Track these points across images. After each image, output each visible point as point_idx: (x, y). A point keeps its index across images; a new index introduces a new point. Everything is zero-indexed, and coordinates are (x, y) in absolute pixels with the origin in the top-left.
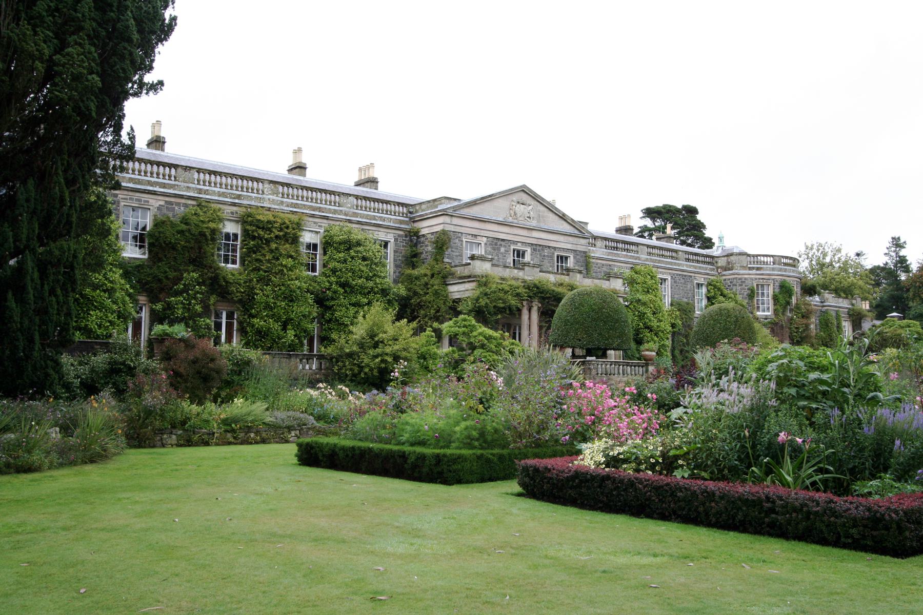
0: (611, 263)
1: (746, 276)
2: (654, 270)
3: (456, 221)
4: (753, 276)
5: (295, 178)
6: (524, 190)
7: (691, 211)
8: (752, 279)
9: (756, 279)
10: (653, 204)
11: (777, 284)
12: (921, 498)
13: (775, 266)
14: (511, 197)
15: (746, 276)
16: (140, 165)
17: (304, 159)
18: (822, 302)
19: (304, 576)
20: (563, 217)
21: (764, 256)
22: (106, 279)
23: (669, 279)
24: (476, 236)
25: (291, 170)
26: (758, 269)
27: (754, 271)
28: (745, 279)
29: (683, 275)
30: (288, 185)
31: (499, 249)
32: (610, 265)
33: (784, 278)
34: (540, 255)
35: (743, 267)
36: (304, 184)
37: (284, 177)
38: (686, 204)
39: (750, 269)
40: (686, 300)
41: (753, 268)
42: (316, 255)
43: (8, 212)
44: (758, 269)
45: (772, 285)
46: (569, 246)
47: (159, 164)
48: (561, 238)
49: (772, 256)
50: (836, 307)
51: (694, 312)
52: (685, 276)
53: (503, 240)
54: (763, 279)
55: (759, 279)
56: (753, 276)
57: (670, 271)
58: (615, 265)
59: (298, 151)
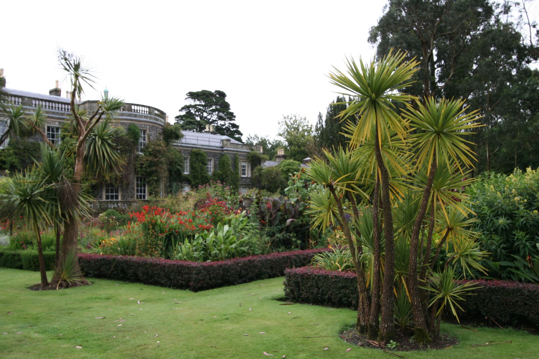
5: (54, 97)
7: (222, 95)
10: (195, 90)
13: (124, 112)
16: (18, 99)
18: (222, 147)
19: (414, 325)
21: (137, 105)
25: (51, 92)
30: (52, 102)
33: (133, 122)
36: (60, 101)
37: (48, 97)
42: (245, 170)
43: (475, 199)
47: (58, 103)
49: (149, 107)
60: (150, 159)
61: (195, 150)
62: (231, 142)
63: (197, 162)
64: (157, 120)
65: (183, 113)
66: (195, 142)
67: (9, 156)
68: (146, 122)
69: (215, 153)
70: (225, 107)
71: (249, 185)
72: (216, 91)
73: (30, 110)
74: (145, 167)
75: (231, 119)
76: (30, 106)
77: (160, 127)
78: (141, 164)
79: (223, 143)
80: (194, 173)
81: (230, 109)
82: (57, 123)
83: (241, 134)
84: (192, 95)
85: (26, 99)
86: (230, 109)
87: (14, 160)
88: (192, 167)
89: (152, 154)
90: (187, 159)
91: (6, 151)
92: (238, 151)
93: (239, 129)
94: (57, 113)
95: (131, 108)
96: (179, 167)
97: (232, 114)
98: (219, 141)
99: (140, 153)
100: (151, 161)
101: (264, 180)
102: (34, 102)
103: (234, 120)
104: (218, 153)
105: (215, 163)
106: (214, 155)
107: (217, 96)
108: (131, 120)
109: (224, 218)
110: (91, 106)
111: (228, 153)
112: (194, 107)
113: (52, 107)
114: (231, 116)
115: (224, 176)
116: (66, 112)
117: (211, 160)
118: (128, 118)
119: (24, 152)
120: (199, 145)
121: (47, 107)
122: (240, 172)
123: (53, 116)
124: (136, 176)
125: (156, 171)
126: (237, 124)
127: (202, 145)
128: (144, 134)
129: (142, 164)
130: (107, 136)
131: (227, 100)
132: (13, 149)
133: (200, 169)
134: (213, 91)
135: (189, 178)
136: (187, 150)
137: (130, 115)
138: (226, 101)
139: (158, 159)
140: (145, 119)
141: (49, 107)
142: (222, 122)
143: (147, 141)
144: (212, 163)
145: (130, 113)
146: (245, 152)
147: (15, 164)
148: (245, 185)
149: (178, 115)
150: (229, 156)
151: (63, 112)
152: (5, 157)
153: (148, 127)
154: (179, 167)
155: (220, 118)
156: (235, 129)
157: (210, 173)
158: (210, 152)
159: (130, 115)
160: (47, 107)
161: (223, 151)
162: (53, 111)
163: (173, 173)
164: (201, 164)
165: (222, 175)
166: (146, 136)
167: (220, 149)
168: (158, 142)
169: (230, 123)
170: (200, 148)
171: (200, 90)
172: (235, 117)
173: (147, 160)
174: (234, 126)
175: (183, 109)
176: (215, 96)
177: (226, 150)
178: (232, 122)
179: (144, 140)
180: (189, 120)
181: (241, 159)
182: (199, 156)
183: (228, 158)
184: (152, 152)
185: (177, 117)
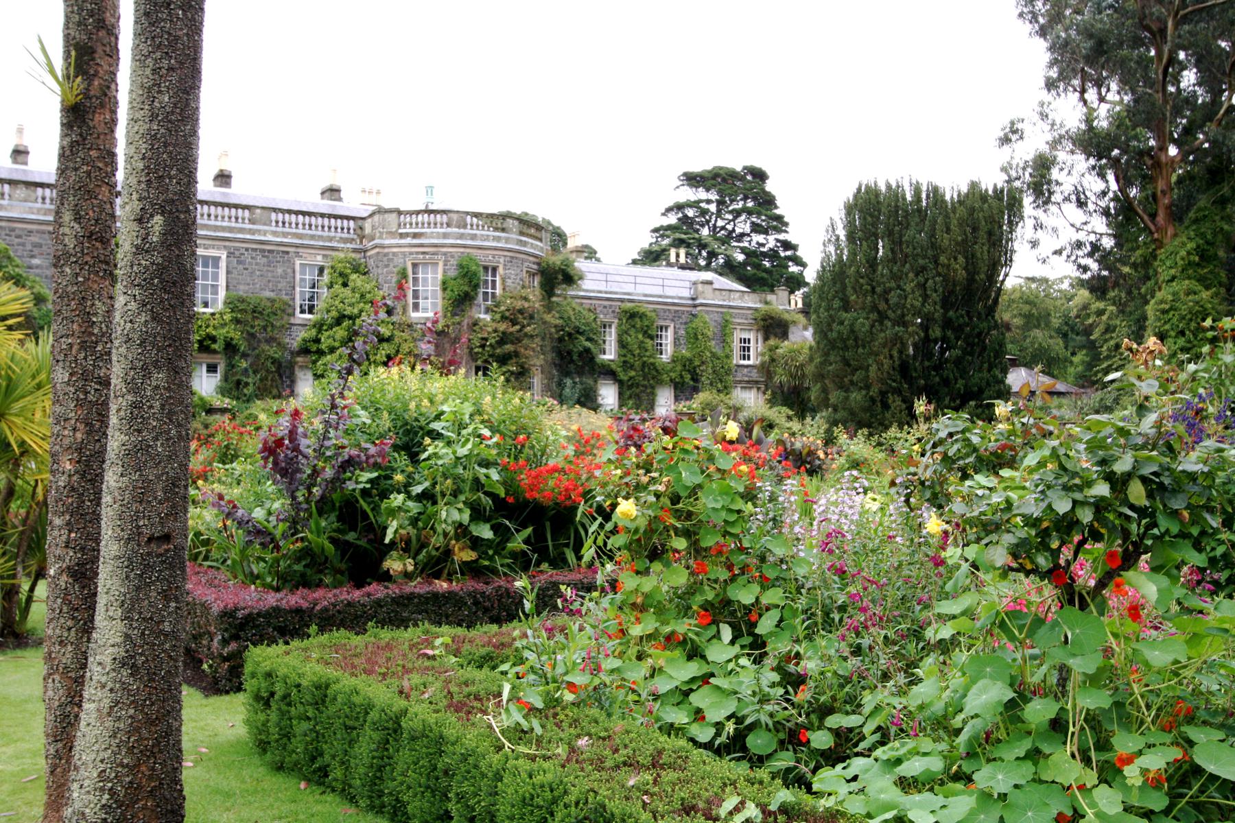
1: (395, 250)
4: (406, 250)
5: (326, 206)
8: (404, 254)
9: (411, 253)
10: (697, 167)
11: (453, 262)
12: (492, 820)
13: (449, 230)
15: (395, 250)
17: (27, 141)
18: (693, 299)
23: (224, 257)
26: (415, 236)
27: (409, 240)
28: (394, 254)
29: (264, 251)
35: (392, 234)
38: (748, 164)
39: (402, 236)
40: (268, 294)
41: (407, 235)
44: (415, 236)
45: (441, 264)
50: (721, 306)
51: (293, 315)
52: (269, 251)
54: (424, 253)
55: (417, 253)
57: (227, 244)
59: (20, 131)
60: (502, 327)
61: (629, 305)
62: (716, 286)
63: (632, 332)
64: (525, 244)
65: (672, 219)
66: (629, 288)
67: (223, 325)
68: (496, 249)
69: (676, 311)
70: (768, 201)
71: (757, 382)
72: (745, 168)
73: (265, 233)
74: (491, 345)
75: (779, 231)
76: (265, 224)
77: (531, 259)
78: (483, 339)
79: (696, 289)
80: (625, 356)
81: (776, 207)
82: (319, 258)
83: (804, 265)
84: (693, 179)
85: (258, 211)
86: (776, 207)
87: (232, 335)
88: (622, 344)
89: (507, 318)
90: (610, 326)
91: (217, 316)
92: (730, 307)
93: (798, 253)
94: (321, 238)
95: (465, 221)
96: (588, 344)
97: (779, 218)
98: (688, 284)
99: (482, 316)
100: (504, 333)
101: (779, 370)
102: (273, 216)
103: (786, 232)
104: (683, 312)
105: (675, 333)
106: (676, 316)
107: (749, 178)
108: (465, 246)
109: (212, 369)
110: (384, 220)
111: (707, 312)
112: (695, 204)
113: (310, 225)
114: (779, 223)
115: (697, 363)
116: (339, 235)
117: (667, 328)
118: (459, 242)
119: (254, 318)
120: (638, 295)
121: (300, 226)
122: (736, 352)
123: (312, 243)
124: (474, 365)
125: (516, 354)
126: (794, 242)
127: (646, 295)
128: (494, 275)
129: (486, 339)
130: (850, 266)
131: (770, 186)
132: (232, 311)
133: (640, 347)
134: (739, 168)
135: (613, 366)
136: (611, 306)
137: (461, 236)
138: (767, 189)
139: (518, 327)
140: (494, 244)
141: (304, 225)
142: (760, 238)
143: (498, 291)
144: (670, 334)
145: (462, 231)
146: (749, 308)
147: (234, 342)
148: (748, 382)
149: (658, 225)
150: (707, 318)
151: (332, 234)
152: (215, 328)
153: (502, 260)
154: (588, 344)
155: (756, 229)
156: (789, 253)
157: (665, 358)
158: (665, 311)
159: (461, 236)
160: (300, 226)
161: (695, 306)
162: (313, 232)
163: (575, 357)
164: (640, 336)
165: (691, 361)
166: (498, 279)
167: (690, 302)
168: (524, 293)
169: (778, 240)
170: (640, 301)
171: (709, 168)
172: (786, 224)
173: (495, 331)
174: (787, 245)
175: (669, 210)
176: (742, 179)
177: (702, 305)
178: (782, 237)
179: (494, 287)
180: (678, 235)
181: (739, 324)
182: (637, 320)
183: (705, 323)
184: (507, 314)
185: (656, 230)
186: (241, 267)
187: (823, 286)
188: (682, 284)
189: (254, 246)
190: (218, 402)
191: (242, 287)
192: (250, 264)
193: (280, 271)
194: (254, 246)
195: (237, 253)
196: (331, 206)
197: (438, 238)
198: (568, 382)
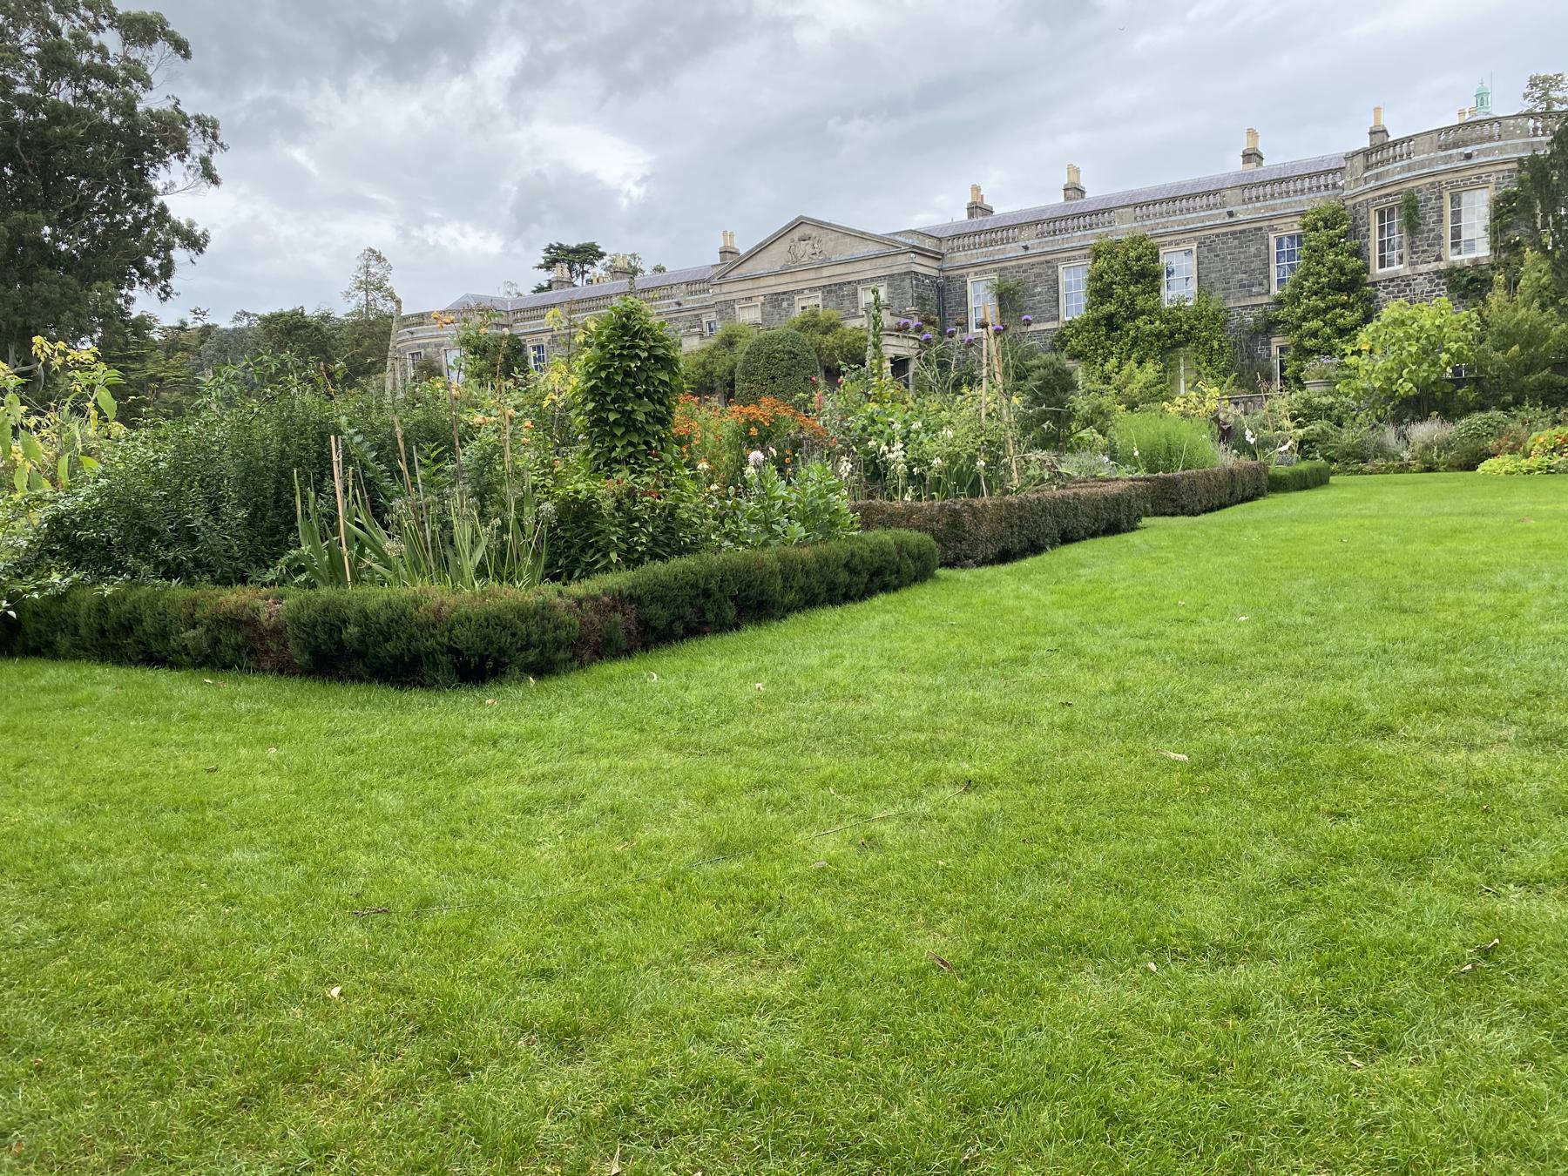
0: (1049, 258)
2: (401, 395)
3: (726, 288)
4: (1370, 195)
5: (980, 221)
6: (800, 223)
9: (1374, 199)
14: (789, 237)
20: (863, 237)
22: (876, 346)
24: (750, 298)
29: (1235, 233)
31: (780, 305)
32: (1047, 262)
34: (837, 297)
44: (1377, 177)
46: (880, 273)
48: (867, 265)
53: (784, 293)
54: (1387, 195)
55: (1380, 197)
56: (1370, 195)
57: (1197, 234)
58: (1058, 259)
82: (1296, 226)
108: (1433, 174)
138: (120, 12)
186: (1212, 255)
187: (109, 78)
188: (1510, 166)
189: (1224, 230)
190: (1012, 405)
191: (1213, 275)
192: (1221, 249)
193: (1253, 250)
194: (1224, 230)
195: (1208, 241)
196: (542, 297)
197: (1399, 173)
198: (910, 489)
